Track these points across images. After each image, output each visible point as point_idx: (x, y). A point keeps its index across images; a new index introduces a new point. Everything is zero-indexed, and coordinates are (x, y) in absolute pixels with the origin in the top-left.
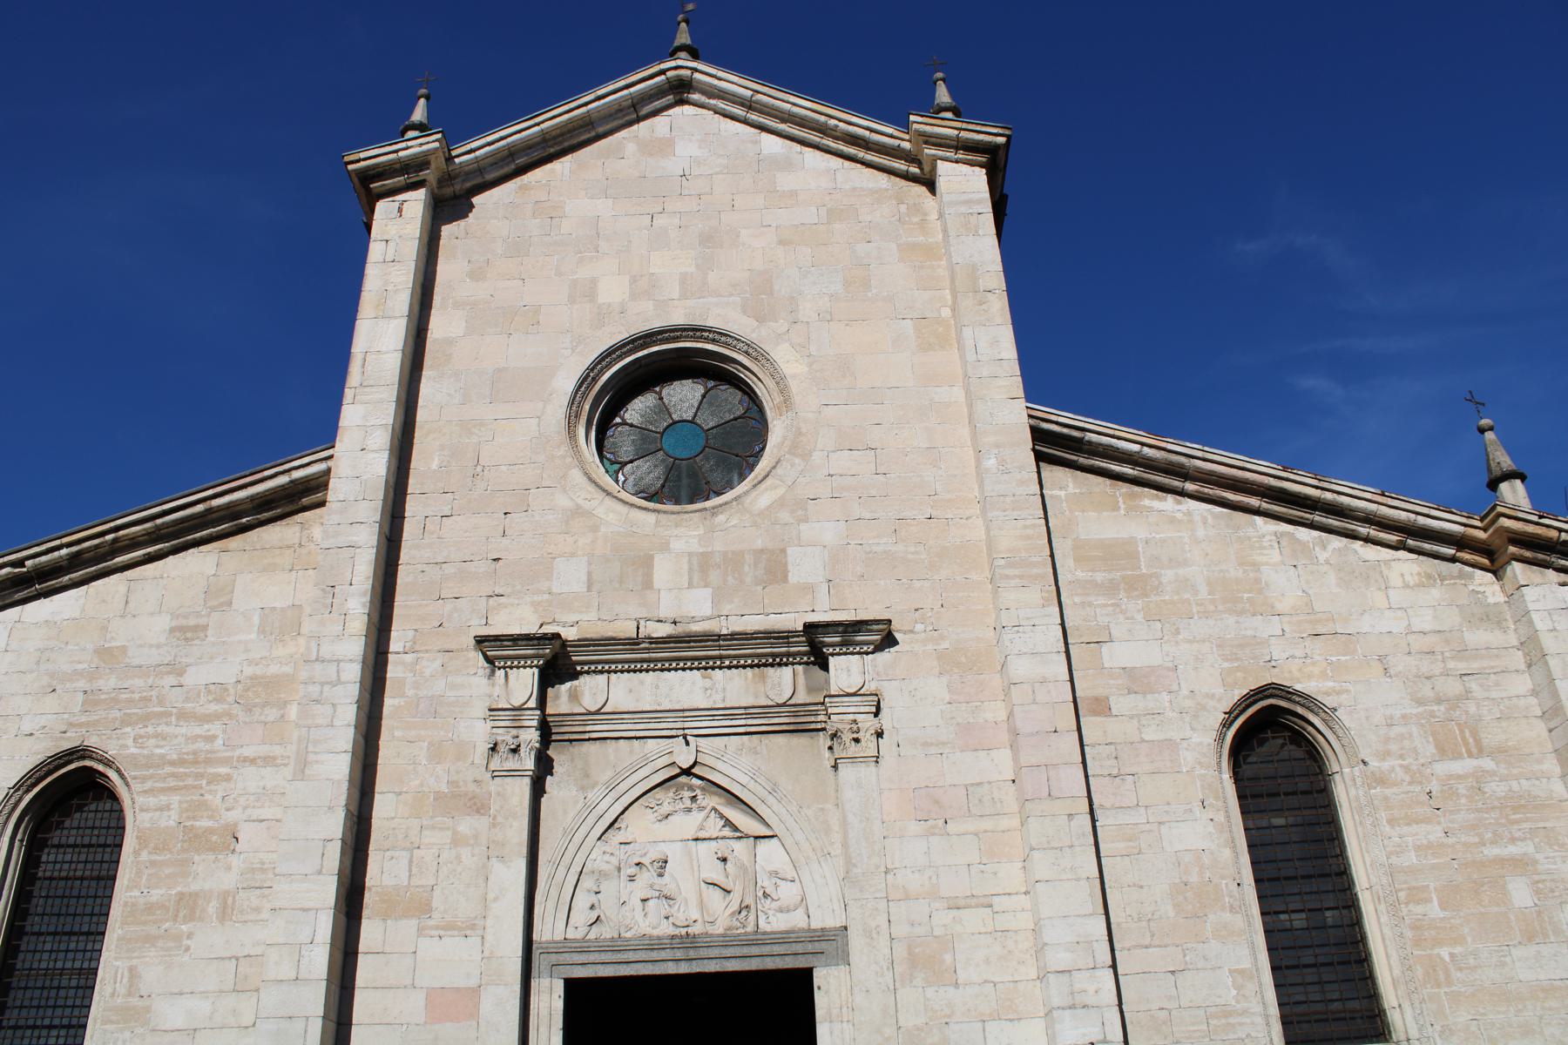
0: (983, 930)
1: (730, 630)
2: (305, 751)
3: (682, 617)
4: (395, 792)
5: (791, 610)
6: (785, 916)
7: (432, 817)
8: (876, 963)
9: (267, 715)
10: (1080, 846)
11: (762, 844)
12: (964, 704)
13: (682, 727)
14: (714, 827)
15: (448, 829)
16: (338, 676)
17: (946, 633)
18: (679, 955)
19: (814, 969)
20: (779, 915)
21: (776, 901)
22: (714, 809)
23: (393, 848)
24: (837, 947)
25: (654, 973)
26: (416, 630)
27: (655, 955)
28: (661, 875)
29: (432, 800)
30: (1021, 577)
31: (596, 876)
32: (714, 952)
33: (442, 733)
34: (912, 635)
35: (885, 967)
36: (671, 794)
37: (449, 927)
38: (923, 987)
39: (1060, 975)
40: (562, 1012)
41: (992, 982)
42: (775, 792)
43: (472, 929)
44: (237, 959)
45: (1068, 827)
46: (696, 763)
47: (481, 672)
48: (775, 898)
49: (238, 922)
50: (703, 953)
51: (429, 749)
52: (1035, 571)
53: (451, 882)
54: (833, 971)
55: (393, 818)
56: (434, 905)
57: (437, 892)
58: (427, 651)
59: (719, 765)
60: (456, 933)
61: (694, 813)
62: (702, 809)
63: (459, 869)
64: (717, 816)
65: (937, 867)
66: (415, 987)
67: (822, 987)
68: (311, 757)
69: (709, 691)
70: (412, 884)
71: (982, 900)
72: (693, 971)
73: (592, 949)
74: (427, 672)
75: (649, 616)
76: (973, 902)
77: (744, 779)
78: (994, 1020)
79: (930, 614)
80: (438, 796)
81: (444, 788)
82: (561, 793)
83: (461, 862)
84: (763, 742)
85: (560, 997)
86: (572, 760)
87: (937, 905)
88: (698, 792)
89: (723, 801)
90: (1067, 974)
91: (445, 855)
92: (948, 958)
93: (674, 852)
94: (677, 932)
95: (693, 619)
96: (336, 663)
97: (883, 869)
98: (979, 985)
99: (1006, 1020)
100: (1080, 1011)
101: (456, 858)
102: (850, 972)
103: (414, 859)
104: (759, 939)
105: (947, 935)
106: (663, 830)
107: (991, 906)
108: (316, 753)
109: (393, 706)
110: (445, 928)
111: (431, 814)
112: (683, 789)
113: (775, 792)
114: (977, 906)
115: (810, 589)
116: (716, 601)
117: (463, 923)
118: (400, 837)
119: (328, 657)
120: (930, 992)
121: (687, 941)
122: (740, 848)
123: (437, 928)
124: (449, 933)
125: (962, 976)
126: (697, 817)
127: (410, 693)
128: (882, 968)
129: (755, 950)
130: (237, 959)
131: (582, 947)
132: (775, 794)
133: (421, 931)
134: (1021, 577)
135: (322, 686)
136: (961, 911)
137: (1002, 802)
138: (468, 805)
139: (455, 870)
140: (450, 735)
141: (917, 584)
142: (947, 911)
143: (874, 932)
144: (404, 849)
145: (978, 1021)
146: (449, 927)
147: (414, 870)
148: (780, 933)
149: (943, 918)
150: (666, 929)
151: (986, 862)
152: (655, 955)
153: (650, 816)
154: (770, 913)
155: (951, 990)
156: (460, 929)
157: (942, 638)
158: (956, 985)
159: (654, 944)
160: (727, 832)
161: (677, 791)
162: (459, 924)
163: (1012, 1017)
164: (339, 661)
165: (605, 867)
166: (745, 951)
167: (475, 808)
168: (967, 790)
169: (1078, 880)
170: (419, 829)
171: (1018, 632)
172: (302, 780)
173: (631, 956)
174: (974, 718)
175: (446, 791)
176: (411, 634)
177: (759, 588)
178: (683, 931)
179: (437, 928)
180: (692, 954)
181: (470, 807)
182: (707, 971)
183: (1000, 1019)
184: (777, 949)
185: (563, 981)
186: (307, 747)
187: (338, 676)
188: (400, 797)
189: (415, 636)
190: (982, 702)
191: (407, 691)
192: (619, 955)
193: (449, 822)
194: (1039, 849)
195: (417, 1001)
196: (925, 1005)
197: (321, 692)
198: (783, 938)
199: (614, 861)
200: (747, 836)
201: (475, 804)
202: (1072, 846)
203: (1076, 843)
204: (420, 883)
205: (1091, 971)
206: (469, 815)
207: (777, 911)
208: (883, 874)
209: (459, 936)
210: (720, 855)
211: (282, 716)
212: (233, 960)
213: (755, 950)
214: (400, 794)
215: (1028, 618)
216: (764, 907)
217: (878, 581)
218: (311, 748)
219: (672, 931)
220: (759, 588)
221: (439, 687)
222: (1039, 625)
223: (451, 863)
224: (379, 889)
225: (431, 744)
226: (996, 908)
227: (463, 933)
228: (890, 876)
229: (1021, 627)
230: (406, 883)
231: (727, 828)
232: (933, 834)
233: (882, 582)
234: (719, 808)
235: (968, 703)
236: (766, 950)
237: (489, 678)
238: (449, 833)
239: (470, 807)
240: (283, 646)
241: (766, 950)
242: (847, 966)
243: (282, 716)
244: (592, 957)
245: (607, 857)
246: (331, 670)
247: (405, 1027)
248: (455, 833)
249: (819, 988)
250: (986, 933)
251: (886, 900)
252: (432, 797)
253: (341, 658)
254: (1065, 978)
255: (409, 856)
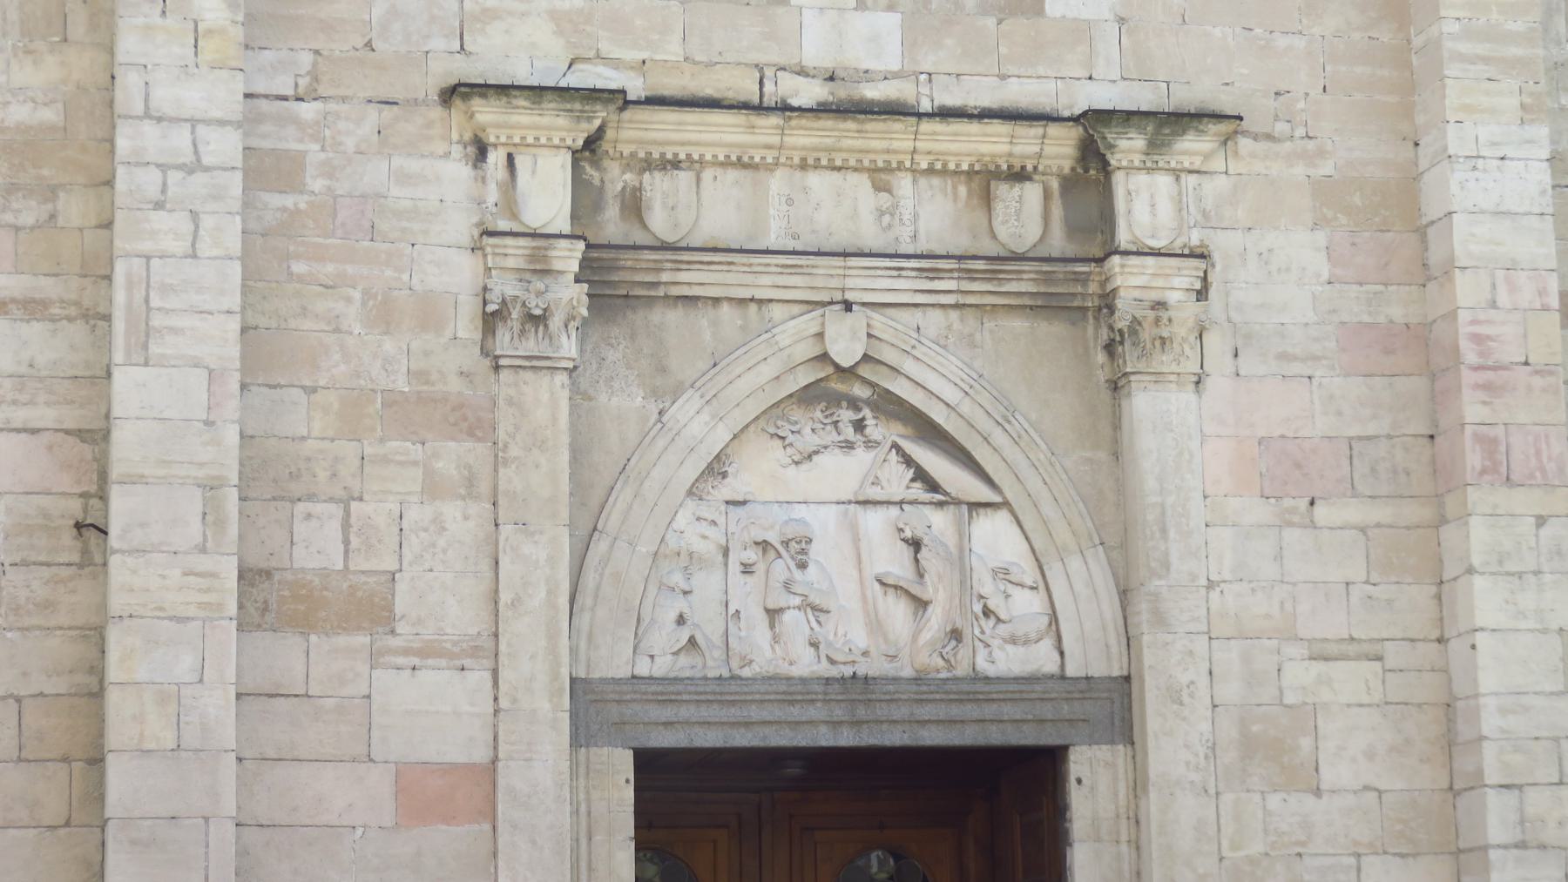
0: (1365, 700)
1: (936, 103)
2: (144, 307)
3: (846, 69)
4: (303, 387)
5: (1050, 73)
6: (1021, 650)
7: (382, 440)
8: (1186, 746)
9: (19, 211)
10: (1551, 573)
11: (981, 517)
12: (1355, 287)
13: (748, 263)
14: (897, 480)
15: (415, 463)
16: (196, 152)
17: (1329, 146)
18: (839, 712)
19: (1071, 748)
20: (1010, 648)
21: (1004, 622)
22: (895, 446)
23: (311, 497)
24: (1113, 712)
25: (795, 743)
26: (317, 52)
27: (795, 712)
28: (802, 566)
29: (379, 405)
30: (1486, 60)
31: (684, 559)
32: (901, 712)
33: (389, 273)
34: (1270, 144)
35: (1202, 756)
36: (818, 414)
37: (428, 651)
38: (1262, 793)
39: (1503, 790)
40: (632, 809)
41: (1376, 790)
42: (1009, 422)
43: (472, 656)
44: (18, 700)
45: (1534, 538)
46: (866, 358)
47: (457, 150)
48: (1002, 617)
49: (11, 630)
50: (882, 711)
51: (364, 304)
52: (1515, 51)
53: (427, 566)
54: (1102, 752)
55: (303, 438)
56: (399, 610)
57: (402, 587)
58: (344, 99)
59: (909, 366)
60: (443, 662)
61: (860, 452)
62: (870, 444)
63: (442, 543)
64: (901, 460)
65: (1294, 584)
66: (371, 760)
67: (1084, 781)
68: (157, 321)
69: (886, 219)
70: (352, 567)
71: (1366, 648)
72: (863, 744)
73: (685, 697)
74: (350, 144)
75: (782, 61)
76: (1352, 649)
77: (952, 395)
78: (1377, 854)
79: (1301, 105)
80: (392, 401)
81: (402, 385)
82: (615, 399)
83: (444, 529)
84: (987, 325)
85: (627, 781)
86: (633, 337)
87: (1292, 650)
88: (867, 412)
89: (909, 431)
90: (1516, 792)
91: (413, 514)
92: (1306, 743)
93: (823, 523)
94: (834, 672)
95: (867, 75)
96: (188, 125)
97: (1204, 582)
98: (1355, 792)
99: (1395, 854)
100: (1532, 854)
101: (434, 521)
102: (1134, 757)
103: (353, 520)
104: (979, 688)
105: (1306, 704)
106: (803, 480)
107: (1379, 658)
108: (167, 311)
109: (284, 209)
110: (423, 653)
111: (379, 433)
112: (839, 406)
113: (1009, 422)
114: (1358, 658)
115: (1081, 32)
116: (909, 44)
117: (455, 643)
118: (323, 475)
119: (168, 110)
120: (1274, 801)
121: (856, 689)
122: (940, 522)
123: (407, 652)
124: (430, 662)
125: (1328, 777)
126: (862, 457)
127: (317, 185)
128: (1197, 755)
129: (971, 711)
130: (18, 700)
131: (666, 690)
132: (1007, 426)
133: (375, 658)
134: (1486, 60)
135: (164, 173)
136: (1331, 664)
137: (1408, 474)
138: (452, 420)
139: (434, 545)
140: (406, 277)
141: (1281, 42)
142: (1307, 662)
143: (1185, 693)
144: (331, 500)
145: (1349, 855)
146: (428, 651)
147: (355, 542)
148: (1017, 680)
149: (1300, 675)
150: (806, 664)
151: (1379, 580)
152: (795, 712)
153: (776, 451)
154: (995, 643)
155: (1310, 800)
156: (451, 656)
157: (1321, 153)
158: (1318, 792)
159: (793, 691)
160: (918, 491)
161: (827, 408)
162: (448, 645)
163: (1405, 851)
164: (194, 122)
165: (699, 546)
166: (955, 711)
167: (464, 425)
168: (1351, 448)
169: (1544, 631)
170: (357, 462)
171: (1475, 168)
172: (146, 364)
173: (755, 713)
174: (1370, 314)
175: (407, 389)
176: (306, 59)
177: (991, 22)
178: (848, 671)
179: (407, 652)
180: (861, 712)
181: (455, 424)
182: (887, 743)
183: (1385, 853)
184: (1009, 711)
185: (632, 752)
186: (147, 301)
187: (196, 152)
188: (312, 397)
189: (315, 64)
190: (1386, 285)
191: (308, 180)
192: (733, 710)
193: (416, 451)
194: (1484, 573)
195: (379, 781)
196: (1264, 822)
197: (165, 184)
198: (1021, 692)
199: (716, 535)
200: (957, 502)
201: (465, 419)
202: (1540, 572)
203: (1546, 568)
204: (366, 566)
205: (1554, 787)
206: (453, 439)
207: (1005, 641)
208: (1203, 591)
209: (449, 669)
210: (908, 534)
211: (53, 217)
212: (11, 701)
213: (971, 711)
214: (314, 390)
215: (1494, 144)
216: (983, 632)
217: (1209, 28)
218: (155, 302)
219: (824, 669)
220: (991, 22)
221: (375, 174)
222: (1512, 159)
223: (426, 530)
224: (289, 576)
225: (367, 294)
226: (1390, 664)
227: (458, 663)
228: (1214, 595)
229: (1480, 161)
230: (340, 566)
231: (918, 485)
232: (1290, 524)
233: (1217, 32)
234: (911, 448)
235: (1361, 284)
236: (989, 711)
237: (475, 167)
238: (418, 473)
239: (455, 424)
240: (35, 63)
241: (989, 711)
242: (1129, 747)
243: (53, 217)
244: (685, 712)
245: (704, 528)
246: (181, 139)
247: (359, 832)
248: (429, 473)
249: (1079, 781)
250: (1369, 705)
251: (1206, 637)
252: (379, 400)
253: (198, 116)
254: (1511, 798)
255: (341, 513)
